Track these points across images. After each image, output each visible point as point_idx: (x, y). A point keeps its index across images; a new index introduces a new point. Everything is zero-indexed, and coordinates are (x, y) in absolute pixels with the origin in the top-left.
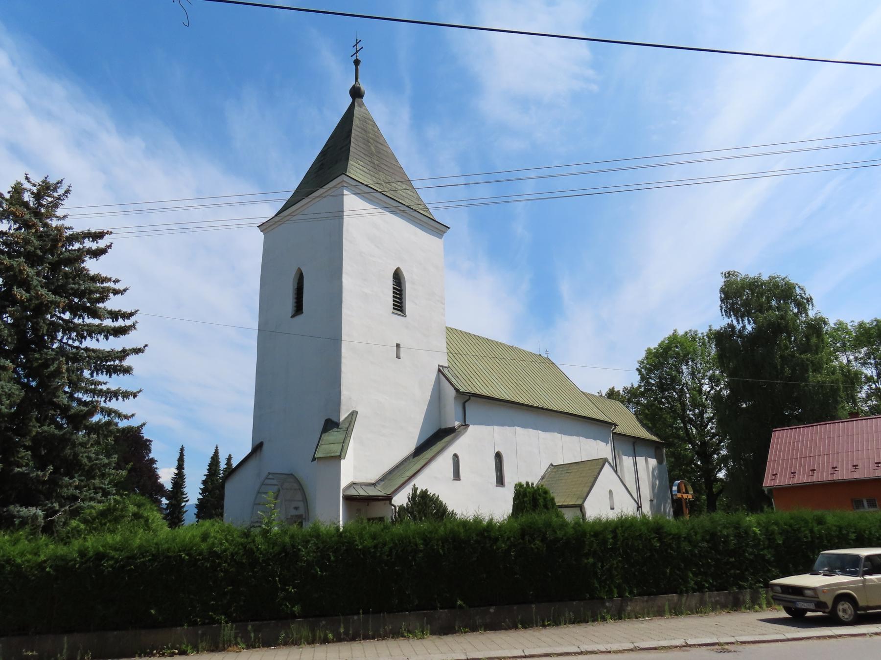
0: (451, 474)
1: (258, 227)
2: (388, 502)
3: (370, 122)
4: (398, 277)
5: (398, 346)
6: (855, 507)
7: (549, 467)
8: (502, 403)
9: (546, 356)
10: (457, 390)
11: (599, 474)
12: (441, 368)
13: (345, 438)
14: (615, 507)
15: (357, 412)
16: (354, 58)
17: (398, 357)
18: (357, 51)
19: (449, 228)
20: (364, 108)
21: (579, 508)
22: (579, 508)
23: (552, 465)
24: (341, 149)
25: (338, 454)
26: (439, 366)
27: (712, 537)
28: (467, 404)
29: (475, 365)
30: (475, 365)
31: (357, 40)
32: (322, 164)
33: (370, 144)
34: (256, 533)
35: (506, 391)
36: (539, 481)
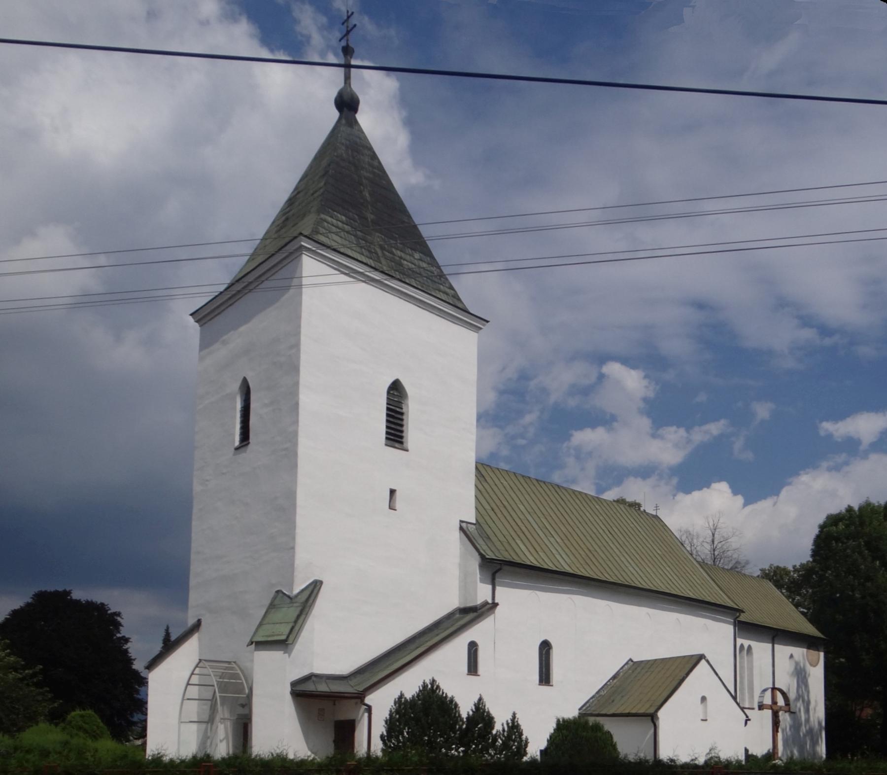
0: (465, 668)
1: (191, 315)
2: (359, 701)
3: (366, 152)
4: (396, 391)
5: (392, 492)
6: (760, 704)
7: (627, 663)
8: (556, 576)
9: (654, 513)
10: (482, 557)
11: (688, 674)
12: (464, 525)
13: (298, 617)
14: (708, 718)
15: (321, 583)
16: (343, 43)
17: (392, 507)
18: (348, 32)
19: (487, 322)
20: (357, 128)
21: (650, 718)
22: (650, 718)
23: (631, 660)
24: (313, 194)
25: (283, 637)
26: (461, 522)
27: (84, 710)
28: (497, 575)
29: (526, 522)
30: (526, 522)
31: (348, 12)
32: (287, 219)
33: (362, 187)
34: (378, 748)
35: (677, 573)
36: (609, 681)
